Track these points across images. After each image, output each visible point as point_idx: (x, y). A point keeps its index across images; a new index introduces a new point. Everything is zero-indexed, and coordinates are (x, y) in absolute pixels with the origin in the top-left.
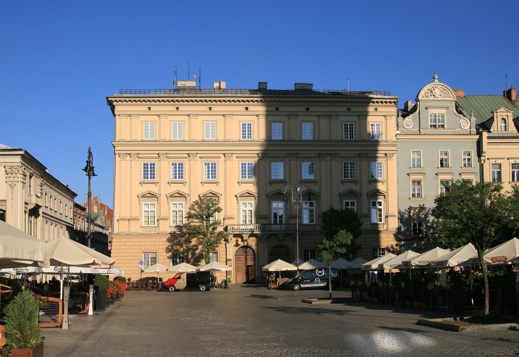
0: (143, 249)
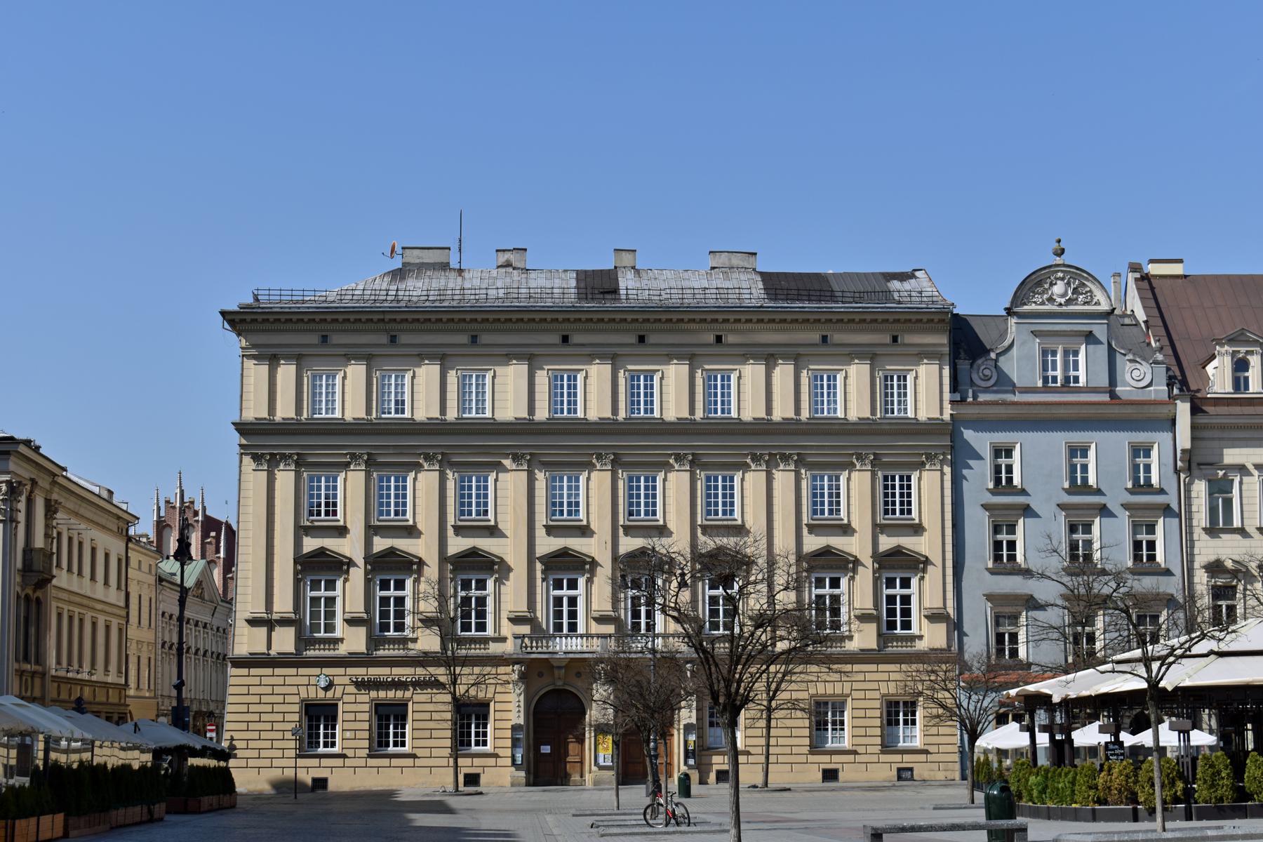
0: (884, 691)
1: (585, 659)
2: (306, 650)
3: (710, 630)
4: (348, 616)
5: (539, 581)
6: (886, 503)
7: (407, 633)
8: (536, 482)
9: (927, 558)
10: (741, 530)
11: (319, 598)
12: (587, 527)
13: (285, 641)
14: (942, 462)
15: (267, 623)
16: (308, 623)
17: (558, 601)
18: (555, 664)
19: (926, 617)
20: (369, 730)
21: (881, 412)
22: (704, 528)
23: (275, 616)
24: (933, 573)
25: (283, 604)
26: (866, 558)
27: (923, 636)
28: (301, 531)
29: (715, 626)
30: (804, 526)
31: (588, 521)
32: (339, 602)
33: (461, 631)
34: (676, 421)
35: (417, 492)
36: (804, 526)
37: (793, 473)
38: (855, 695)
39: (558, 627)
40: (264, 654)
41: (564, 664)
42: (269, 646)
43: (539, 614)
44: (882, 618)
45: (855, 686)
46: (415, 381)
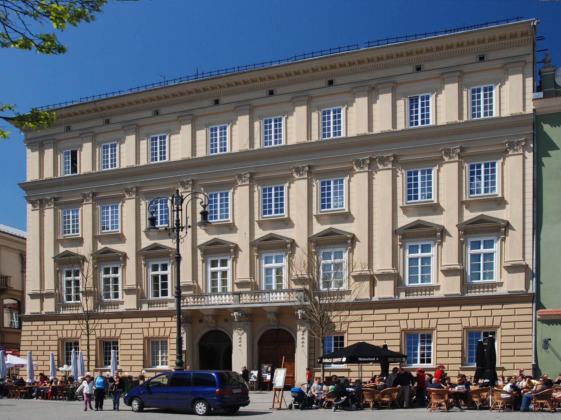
1: (226, 309)
2: (468, 293)
3: (471, 280)
4: (125, 288)
5: (200, 263)
6: (65, 227)
7: (120, 299)
8: (398, 178)
9: (354, 235)
10: (347, 217)
11: (417, 259)
12: (349, 213)
13: (50, 306)
14: (525, 148)
15: (40, 296)
16: (469, 274)
17: (214, 274)
18: (205, 313)
19: (443, 271)
20: (461, 351)
21: (99, 167)
22: (317, 217)
23: (45, 292)
24: (514, 237)
25: (49, 286)
26: (453, 231)
27: (503, 283)
28: (57, 242)
29: (69, 298)
30: (256, 223)
31: (349, 209)
32: (496, 257)
33: (409, 283)
34: (356, 136)
35: (351, 189)
36: (256, 223)
37: (391, 171)
38: (504, 326)
39: (214, 290)
40: (38, 313)
41: (211, 313)
42: (42, 308)
43: (200, 284)
44: (467, 273)
45: (124, 331)
46: (288, 120)
